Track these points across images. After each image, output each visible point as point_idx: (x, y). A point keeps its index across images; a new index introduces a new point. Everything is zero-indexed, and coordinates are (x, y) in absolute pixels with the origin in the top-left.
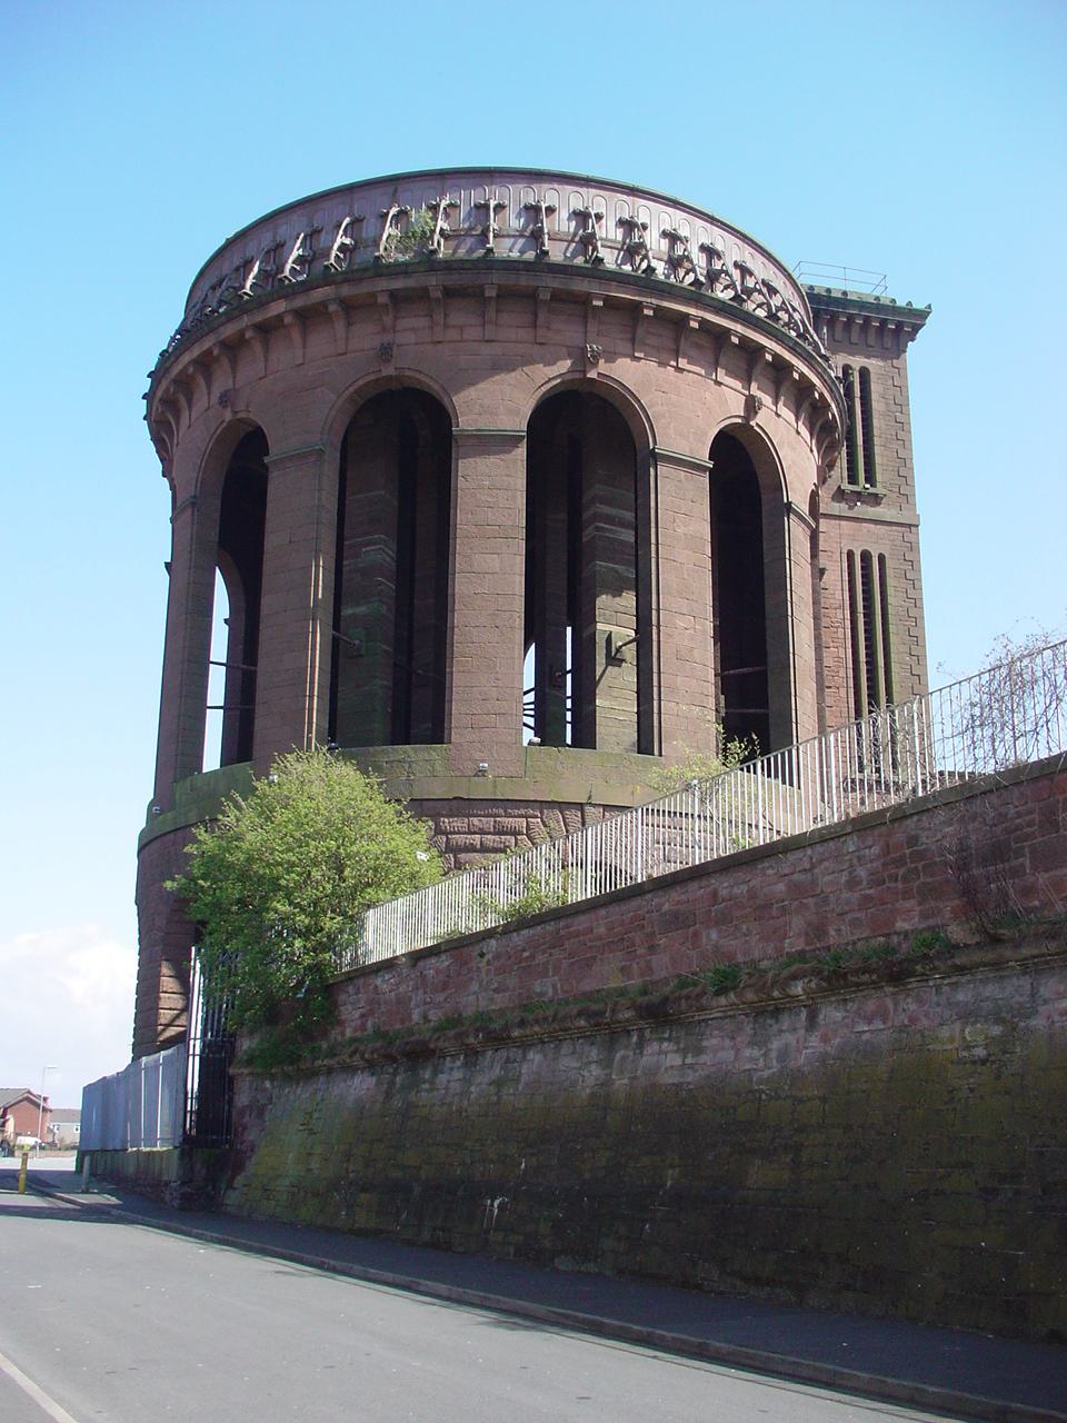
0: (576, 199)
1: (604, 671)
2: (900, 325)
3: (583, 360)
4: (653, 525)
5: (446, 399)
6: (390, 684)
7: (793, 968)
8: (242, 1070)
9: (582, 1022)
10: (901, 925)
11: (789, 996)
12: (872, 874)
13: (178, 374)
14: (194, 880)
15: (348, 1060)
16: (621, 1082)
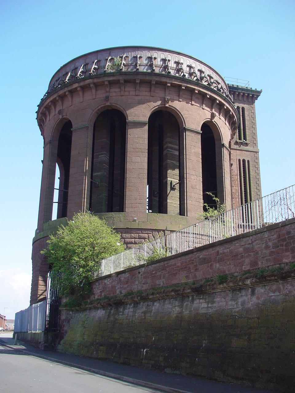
0: (162, 55)
1: (170, 192)
2: (253, 95)
3: (165, 101)
4: (185, 149)
5: (124, 112)
6: (107, 195)
7: (247, 275)
8: (63, 308)
9: (173, 293)
10: (285, 260)
11: (245, 284)
12: (274, 244)
13: (47, 105)
14: (50, 251)
15: (96, 306)
16: (186, 313)
